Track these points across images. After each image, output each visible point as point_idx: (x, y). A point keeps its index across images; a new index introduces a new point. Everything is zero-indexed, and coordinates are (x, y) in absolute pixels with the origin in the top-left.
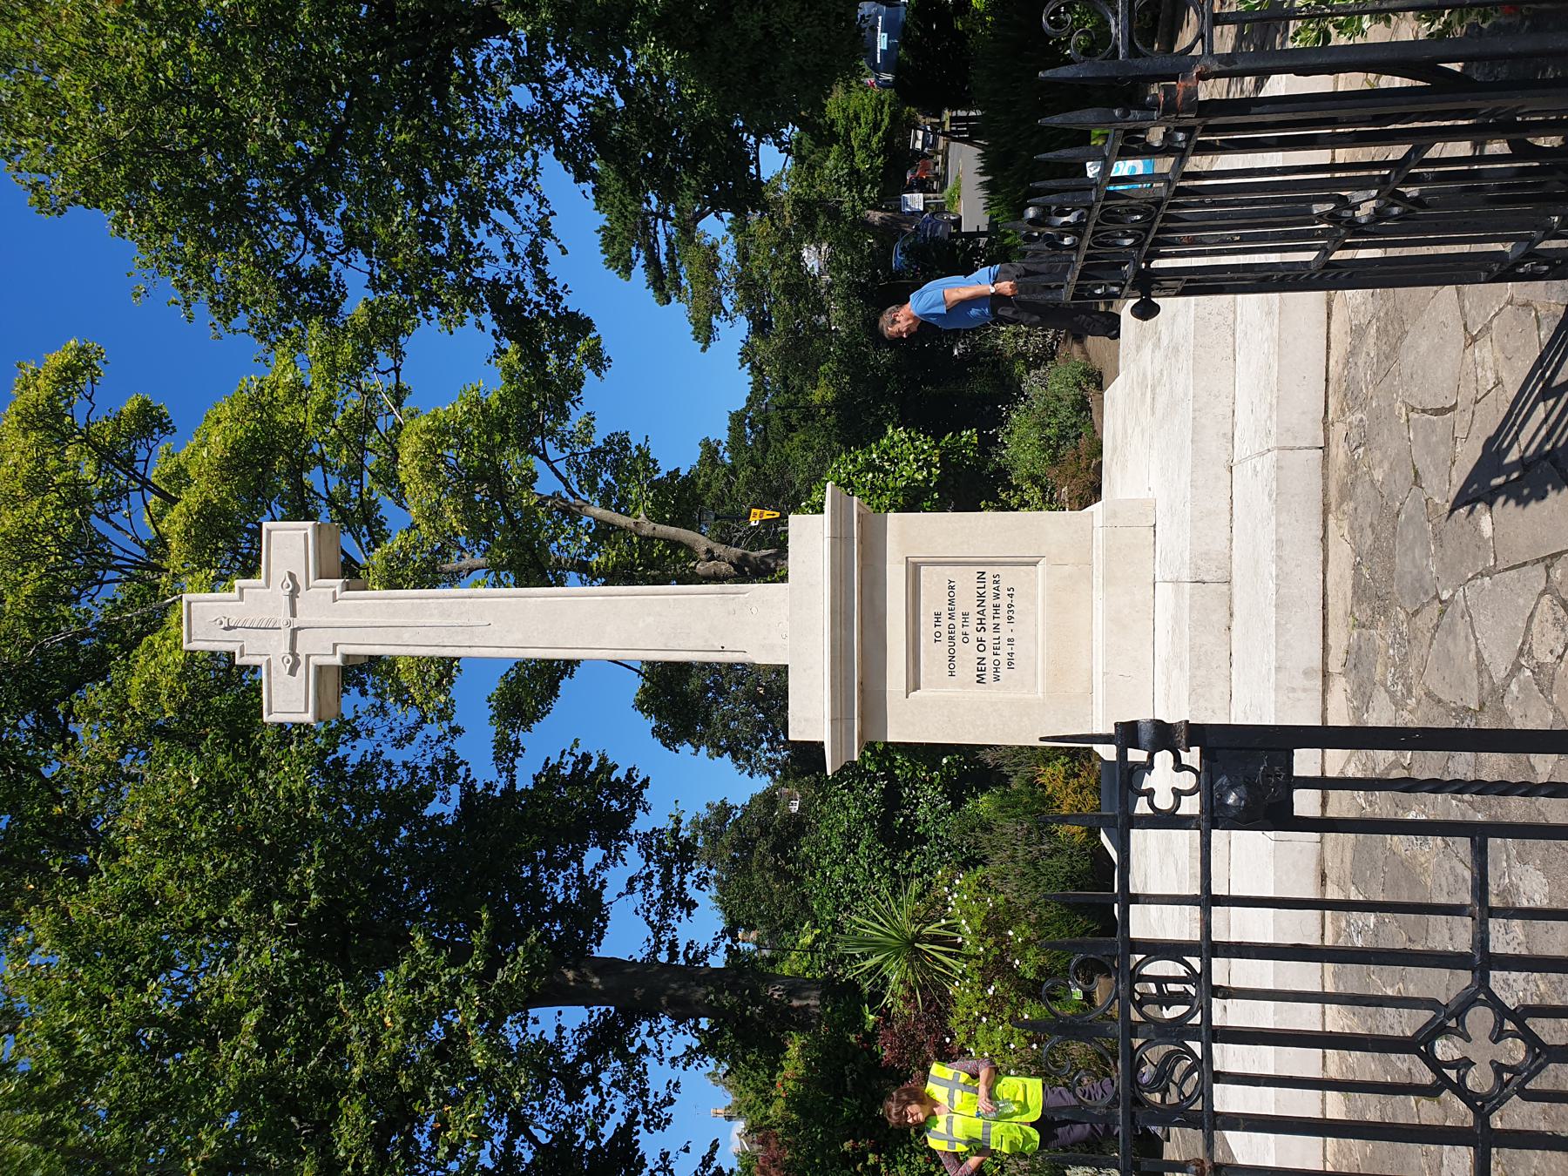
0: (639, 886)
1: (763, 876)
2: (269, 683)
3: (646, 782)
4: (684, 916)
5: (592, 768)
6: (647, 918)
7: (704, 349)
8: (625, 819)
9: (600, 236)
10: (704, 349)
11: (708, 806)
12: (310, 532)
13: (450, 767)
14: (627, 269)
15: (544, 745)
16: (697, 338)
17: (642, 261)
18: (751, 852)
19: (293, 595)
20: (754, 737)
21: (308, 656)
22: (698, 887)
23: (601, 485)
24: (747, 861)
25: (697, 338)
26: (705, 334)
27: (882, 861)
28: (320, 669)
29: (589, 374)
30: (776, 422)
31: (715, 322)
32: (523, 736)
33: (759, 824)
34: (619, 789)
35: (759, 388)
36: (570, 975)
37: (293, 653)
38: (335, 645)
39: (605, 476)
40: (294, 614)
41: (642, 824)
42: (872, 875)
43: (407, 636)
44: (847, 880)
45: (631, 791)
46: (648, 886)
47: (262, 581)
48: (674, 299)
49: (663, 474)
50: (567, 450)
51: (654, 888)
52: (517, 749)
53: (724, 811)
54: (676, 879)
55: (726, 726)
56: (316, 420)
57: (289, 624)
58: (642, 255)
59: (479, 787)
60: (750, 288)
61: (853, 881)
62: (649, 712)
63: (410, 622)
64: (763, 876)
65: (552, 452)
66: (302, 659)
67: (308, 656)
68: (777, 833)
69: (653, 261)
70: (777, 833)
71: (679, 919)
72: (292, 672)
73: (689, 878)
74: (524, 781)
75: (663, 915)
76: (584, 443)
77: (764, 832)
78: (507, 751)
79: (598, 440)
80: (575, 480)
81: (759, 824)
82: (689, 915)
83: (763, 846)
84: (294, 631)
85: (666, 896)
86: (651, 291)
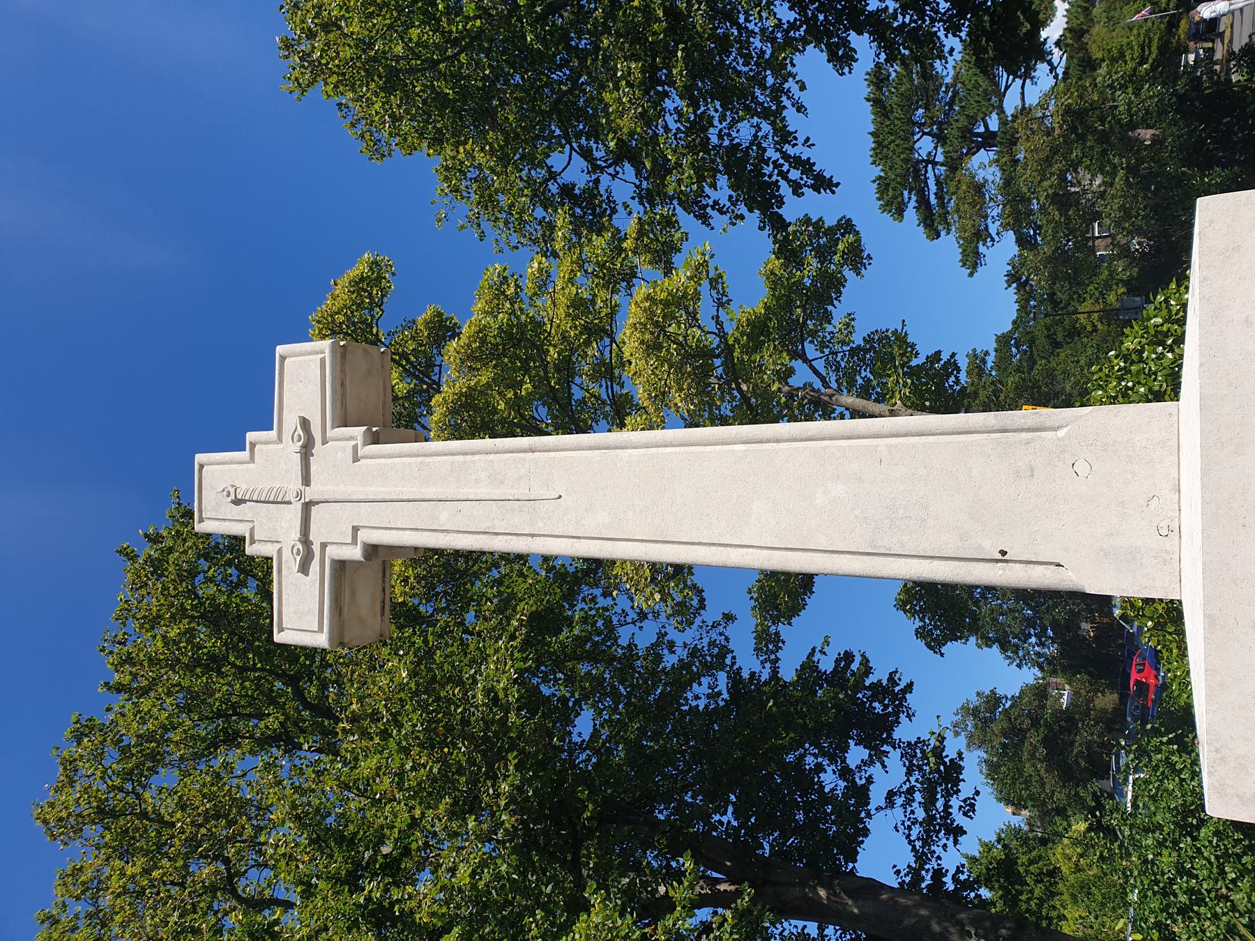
0: (899, 801)
1: (1034, 765)
2: (280, 583)
3: (909, 687)
4: (950, 843)
5: (855, 666)
6: (908, 836)
7: (971, 275)
8: (886, 724)
9: (875, 186)
10: (971, 275)
11: (978, 694)
12: (327, 355)
13: (720, 656)
14: (900, 212)
15: (799, 642)
16: (964, 265)
17: (913, 203)
18: (1022, 741)
19: (307, 451)
20: (1022, 632)
21: (324, 546)
22: (965, 814)
23: (860, 381)
24: (1018, 746)
25: (964, 265)
26: (972, 260)
27: (1239, 857)
28: (341, 567)
29: (848, 273)
30: (1042, 341)
31: (982, 249)
32: (783, 629)
33: (1029, 715)
34: (879, 691)
35: (1023, 308)
36: (822, 893)
37: (306, 540)
38: (355, 529)
39: (863, 374)
40: (306, 481)
41: (905, 731)
42: (1222, 873)
43: (445, 516)
44: (1181, 871)
45: (894, 695)
46: (909, 801)
47: (272, 434)
48: (943, 233)
49: (920, 360)
50: (827, 351)
51: (915, 805)
52: (777, 640)
53: (993, 700)
54: (940, 804)
55: (995, 620)
56: (568, 315)
57: (299, 495)
58: (914, 198)
59: (745, 675)
60: (1018, 218)
61: (1190, 875)
62: (913, 613)
63: (448, 492)
64: (1034, 765)
65: (811, 350)
66: (316, 548)
67: (324, 546)
68: (1049, 727)
69: (923, 202)
70: (1049, 727)
71: (945, 846)
72: (304, 568)
73: (955, 802)
74: (788, 673)
75: (927, 841)
76: (843, 343)
77: (1035, 723)
78: (768, 643)
79: (858, 339)
80: (833, 378)
81: (1029, 715)
82: (956, 842)
83: (1034, 738)
84: (307, 507)
85: (930, 819)
86: (921, 228)
